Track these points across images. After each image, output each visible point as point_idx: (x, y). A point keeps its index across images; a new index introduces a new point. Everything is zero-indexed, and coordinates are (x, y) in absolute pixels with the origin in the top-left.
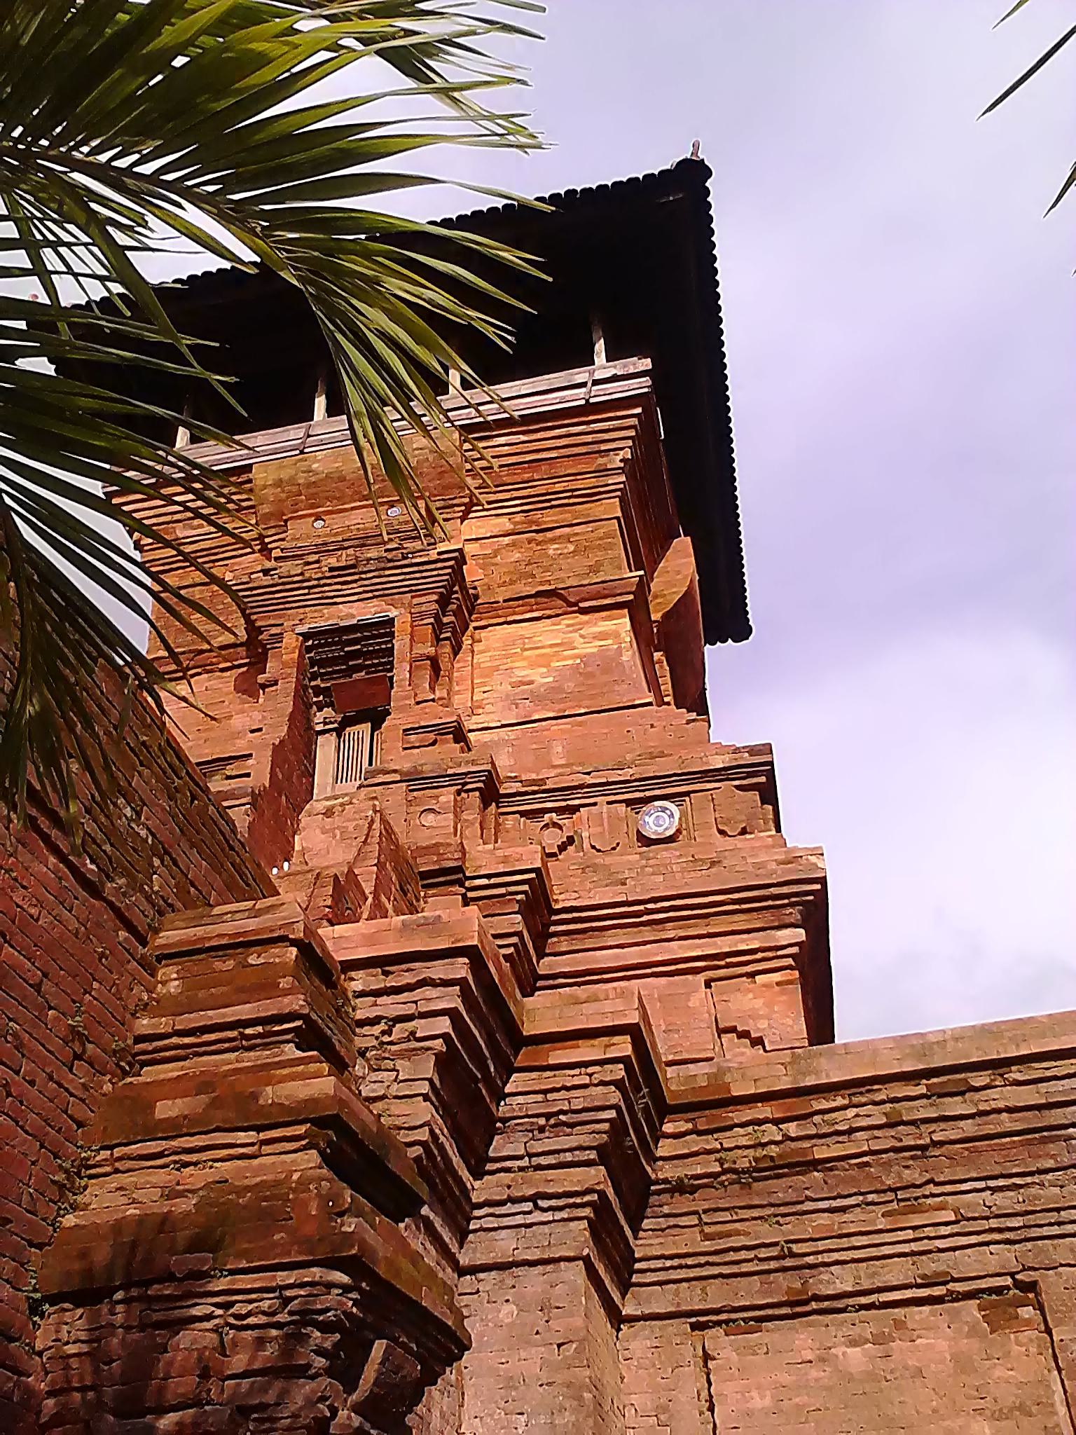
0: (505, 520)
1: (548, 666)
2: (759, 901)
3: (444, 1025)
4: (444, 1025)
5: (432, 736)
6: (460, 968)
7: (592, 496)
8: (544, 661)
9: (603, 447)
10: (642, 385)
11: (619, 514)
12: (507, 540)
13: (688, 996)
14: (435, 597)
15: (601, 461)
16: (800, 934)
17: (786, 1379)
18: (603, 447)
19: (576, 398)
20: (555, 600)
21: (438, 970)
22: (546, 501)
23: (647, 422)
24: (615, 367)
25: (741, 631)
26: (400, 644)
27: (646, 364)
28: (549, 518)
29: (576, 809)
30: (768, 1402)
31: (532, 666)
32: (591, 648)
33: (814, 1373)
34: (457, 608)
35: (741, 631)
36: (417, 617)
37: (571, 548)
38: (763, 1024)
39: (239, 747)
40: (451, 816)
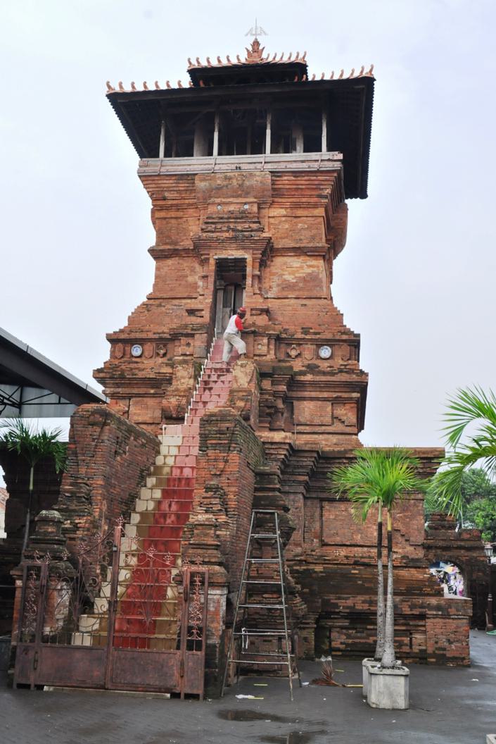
0: (283, 210)
1: (294, 275)
2: (351, 386)
3: (283, 457)
4: (283, 457)
5: (259, 312)
6: (287, 447)
7: (315, 206)
8: (292, 273)
9: (322, 187)
10: (338, 165)
11: (324, 215)
12: (284, 219)
13: (327, 408)
14: (260, 252)
15: (320, 192)
16: (359, 395)
17: (337, 513)
18: (322, 187)
19: (315, 166)
20: (299, 251)
21: (283, 446)
22: (297, 206)
23: (338, 178)
24: (329, 155)
25: (363, 195)
26: (249, 270)
27: (341, 156)
28: (299, 212)
29: (301, 344)
30: (333, 517)
31: (289, 274)
32: (309, 271)
33: (343, 513)
34: (268, 252)
35: (363, 195)
36: (254, 259)
37: (306, 226)
38: (345, 418)
39: (200, 307)
40: (266, 347)
